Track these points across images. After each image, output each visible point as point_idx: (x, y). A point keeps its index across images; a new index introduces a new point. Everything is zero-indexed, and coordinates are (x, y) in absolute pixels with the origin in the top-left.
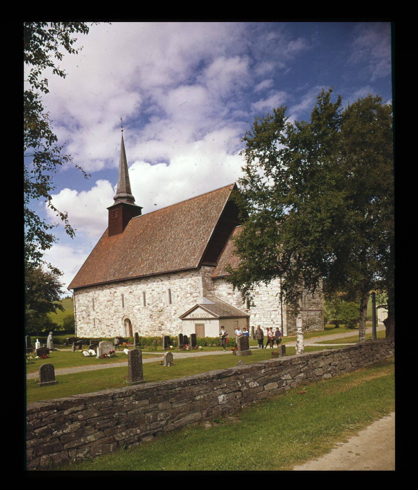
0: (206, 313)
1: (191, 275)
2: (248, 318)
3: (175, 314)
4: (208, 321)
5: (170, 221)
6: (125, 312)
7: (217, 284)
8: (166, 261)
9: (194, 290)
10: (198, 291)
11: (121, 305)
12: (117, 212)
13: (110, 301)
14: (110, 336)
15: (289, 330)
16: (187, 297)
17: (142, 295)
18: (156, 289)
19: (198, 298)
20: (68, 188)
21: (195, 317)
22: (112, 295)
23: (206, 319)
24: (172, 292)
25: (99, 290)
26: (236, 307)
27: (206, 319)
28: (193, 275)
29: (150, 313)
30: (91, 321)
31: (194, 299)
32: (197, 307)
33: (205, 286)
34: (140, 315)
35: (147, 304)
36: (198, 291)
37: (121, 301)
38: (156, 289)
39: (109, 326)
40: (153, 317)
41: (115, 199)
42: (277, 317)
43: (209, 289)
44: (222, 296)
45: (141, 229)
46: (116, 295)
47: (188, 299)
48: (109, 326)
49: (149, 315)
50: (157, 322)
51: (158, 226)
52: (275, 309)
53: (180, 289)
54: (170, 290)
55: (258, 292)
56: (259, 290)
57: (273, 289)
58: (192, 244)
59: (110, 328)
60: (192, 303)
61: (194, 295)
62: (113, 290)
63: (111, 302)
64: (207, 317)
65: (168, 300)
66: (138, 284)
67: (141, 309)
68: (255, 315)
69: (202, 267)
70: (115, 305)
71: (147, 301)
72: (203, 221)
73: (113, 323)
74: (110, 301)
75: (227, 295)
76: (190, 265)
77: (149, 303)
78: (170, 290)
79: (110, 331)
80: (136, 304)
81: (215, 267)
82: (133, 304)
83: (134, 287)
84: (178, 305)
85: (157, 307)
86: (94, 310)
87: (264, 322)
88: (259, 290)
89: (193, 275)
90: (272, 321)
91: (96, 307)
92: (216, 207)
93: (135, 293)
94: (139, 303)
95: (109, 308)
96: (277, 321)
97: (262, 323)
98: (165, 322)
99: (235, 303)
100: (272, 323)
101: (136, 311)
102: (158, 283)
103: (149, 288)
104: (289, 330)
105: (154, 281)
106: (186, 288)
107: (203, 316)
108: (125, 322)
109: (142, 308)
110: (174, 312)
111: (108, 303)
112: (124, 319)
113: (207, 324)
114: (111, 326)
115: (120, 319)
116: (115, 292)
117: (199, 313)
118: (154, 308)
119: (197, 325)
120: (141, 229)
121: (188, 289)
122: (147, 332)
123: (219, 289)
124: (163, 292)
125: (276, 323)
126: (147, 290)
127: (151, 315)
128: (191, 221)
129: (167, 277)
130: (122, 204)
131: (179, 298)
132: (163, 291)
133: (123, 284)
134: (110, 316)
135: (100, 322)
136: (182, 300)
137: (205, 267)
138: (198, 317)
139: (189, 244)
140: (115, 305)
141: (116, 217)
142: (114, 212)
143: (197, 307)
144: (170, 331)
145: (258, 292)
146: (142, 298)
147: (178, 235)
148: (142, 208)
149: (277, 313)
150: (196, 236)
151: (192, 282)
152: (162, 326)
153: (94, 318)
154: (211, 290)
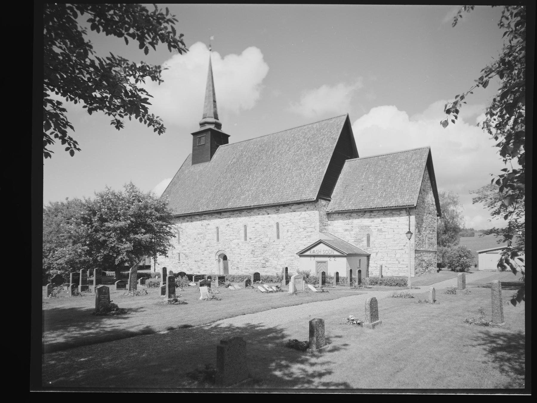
0: (331, 249)
1: (306, 209)
2: (368, 256)
4: (332, 259)
5: (271, 150)
6: (220, 247)
7: (331, 219)
8: (274, 192)
9: (309, 224)
11: (216, 238)
12: (204, 138)
13: (201, 234)
14: (199, 272)
17: (243, 228)
19: (313, 233)
20: (263, 52)
21: (315, 254)
22: (204, 227)
23: (329, 256)
24: (280, 226)
25: (188, 221)
26: (354, 245)
27: (329, 256)
28: (308, 208)
29: (252, 248)
30: (175, 256)
32: (320, 242)
33: (321, 221)
34: (239, 250)
35: (248, 238)
36: (313, 226)
37: (216, 235)
39: (198, 261)
40: (256, 253)
43: (324, 224)
45: (234, 158)
46: (209, 227)
47: (300, 234)
48: (198, 261)
49: (251, 250)
51: (256, 156)
52: (401, 248)
53: (291, 223)
54: (278, 224)
55: (381, 230)
56: (382, 227)
57: (399, 227)
58: (305, 175)
59: (199, 264)
60: (305, 239)
62: (205, 222)
63: (202, 236)
64: (332, 254)
65: (275, 235)
66: (238, 216)
67: (240, 244)
68: (377, 254)
69: (319, 200)
70: (207, 238)
71: (248, 235)
72: (315, 152)
73: (204, 259)
74: (201, 234)
75: (343, 231)
76: (305, 197)
77: (251, 237)
78: (278, 224)
79: (199, 267)
80: (234, 237)
81: (330, 201)
82: (231, 238)
83: (232, 220)
84: (287, 241)
85: (261, 242)
86: (179, 243)
87: (387, 261)
88: (382, 227)
89: (308, 208)
90: (397, 260)
91: (183, 240)
92: (327, 137)
94: (238, 237)
95: (199, 242)
96: (403, 261)
97: (385, 262)
99: (353, 241)
100: (397, 262)
101: (234, 246)
102: (264, 216)
105: (259, 214)
107: (327, 253)
108: (219, 258)
109: (242, 242)
110: (283, 248)
111: (199, 236)
112: (218, 254)
113: (331, 262)
114: (201, 262)
115: (214, 255)
116: (209, 224)
117: (322, 249)
118: (257, 243)
120: (234, 158)
122: (247, 269)
123: (334, 225)
125: (402, 263)
127: (253, 251)
128: (298, 151)
129: (275, 210)
130: (210, 130)
131: (290, 233)
132: (270, 224)
133: (219, 216)
134: (200, 251)
135: (186, 256)
136: (292, 235)
138: (320, 254)
139: (300, 174)
140: (207, 238)
141: (202, 144)
142: (200, 138)
143: (320, 242)
145: (381, 230)
146: (242, 232)
147: (284, 166)
148: (229, 136)
149: (403, 251)
150: (307, 167)
151: (307, 216)
152: (266, 263)
153: (178, 252)
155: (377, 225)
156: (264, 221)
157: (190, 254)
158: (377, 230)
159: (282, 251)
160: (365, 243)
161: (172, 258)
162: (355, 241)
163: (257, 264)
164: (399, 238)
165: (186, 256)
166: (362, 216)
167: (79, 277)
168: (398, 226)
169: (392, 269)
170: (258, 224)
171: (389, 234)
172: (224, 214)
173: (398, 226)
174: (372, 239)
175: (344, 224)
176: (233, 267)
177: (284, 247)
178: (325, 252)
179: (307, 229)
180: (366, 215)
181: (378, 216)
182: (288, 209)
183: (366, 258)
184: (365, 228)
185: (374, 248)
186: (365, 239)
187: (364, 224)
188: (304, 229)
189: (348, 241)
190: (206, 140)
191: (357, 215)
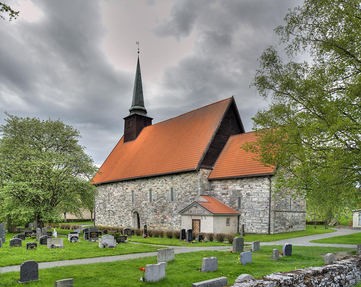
3: (176, 209)
4: (204, 218)
10: (196, 190)
15: (276, 229)
16: (187, 196)
18: (160, 188)
24: (174, 190)
28: (192, 176)
31: (193, 197)
34: (146, 209)
35: (152, 200)
38: (160, 188)
39: (121, 217)
41: (130, 111)
42: (265, 216)
44: (217, 196)
50: (161, 216)
52: (263, 209)
54: (172, 189)
57: (263, 191)
60: (191, 201)
61: (193, 193)
65: (170, 197)
67: (147, 204)
69: (200, 169)
71: (153, 197)
73: (124, 215)
75: (221, 195)
87: (253, 220)
93: (143, 190)
97: (251, 221)
98: (167, 216)
100: (260, 221)
101: (143, 206)
103: (155, 187)
104: (276, 229)
106: (187, 188)
111: (121, 198)
114: (123, 217)
118: (158, 204)
119: (193, 220)
121: (188, 188)
124: (167, 190)
126: (153, 188)
127: (155, 210)
131: (180, 196)
132: (167, 189)
134: (122, 209)
137: (203, 170)
144: (171, 224)
154: (207, 190)
155: (245, 190)
156: (163, 186)
157: (116, 211)
158: (246, 194)
159: (175, 211)
160: (237, 205)
161: (105, 214)
162: (229, 203)
163: (158, 220)
164: (262, 201)
165: (114, 213)
166: (234, 182)
167: (211, 279)
168: (261, 191)
169: (256, 227)
170: (159, 188)
171: (254, 198)
172: (137, 181)
173: (261, 191)
174: (242, 201)
175: (221, 189)
176: (142, 222)
177: (176, 207)
178: (198, 212)
179: (192, 193)
180: (238, 181)
181: (247, 182)
182: (179, 177)
183: (236, 218)
184: (237, 192)
185: (243, 209)
186: (237, 201)
187: (236, 189)
188: (190, 192)
189: (224, 203)
190: (133, 124)
191: (231, 181)
